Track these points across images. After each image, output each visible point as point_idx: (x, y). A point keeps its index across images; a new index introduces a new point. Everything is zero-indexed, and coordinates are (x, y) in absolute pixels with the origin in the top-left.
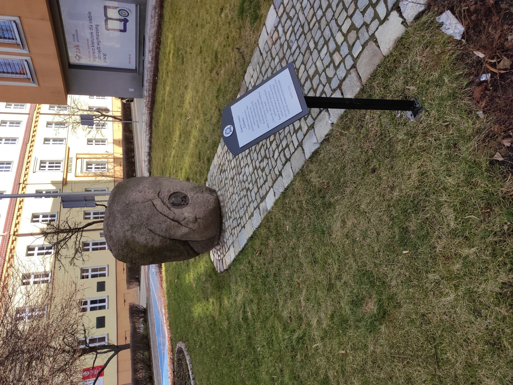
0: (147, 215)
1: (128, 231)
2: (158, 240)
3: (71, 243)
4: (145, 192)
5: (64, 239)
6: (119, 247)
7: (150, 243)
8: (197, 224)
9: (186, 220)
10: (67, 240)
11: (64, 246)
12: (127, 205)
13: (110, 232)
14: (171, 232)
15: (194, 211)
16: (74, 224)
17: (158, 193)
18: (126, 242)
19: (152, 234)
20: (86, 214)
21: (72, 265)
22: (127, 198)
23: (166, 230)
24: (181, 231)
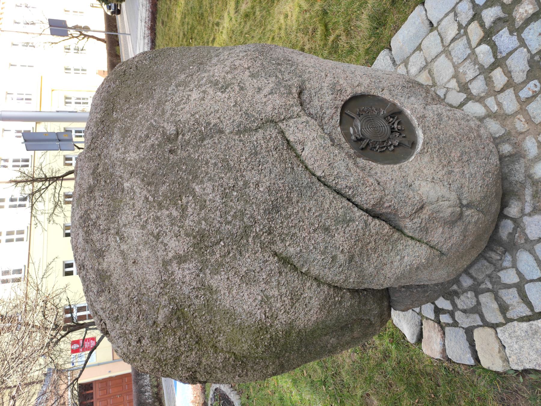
0: (269, 189)
1: (181, 259)
2: (315, 303)
3: (48, 195)
4: (242, 89)
5: (39, 190)
6: (143, 324)
7: (283, 317)
8: (457, 230)
9: (425, 214)
10: (42, 191)
11: (40, 199)
12: (169, 139)
13: (100, 254)
14: (366, 265)
15: (450, 173)
16: (50, 171)
17: (300, 93)
18: (173, 312)
19: (292, 276)
20: (67, 159)
21: (52, 222)
22: (163, 112)
23: (351, 259)
24: (403, 258)
